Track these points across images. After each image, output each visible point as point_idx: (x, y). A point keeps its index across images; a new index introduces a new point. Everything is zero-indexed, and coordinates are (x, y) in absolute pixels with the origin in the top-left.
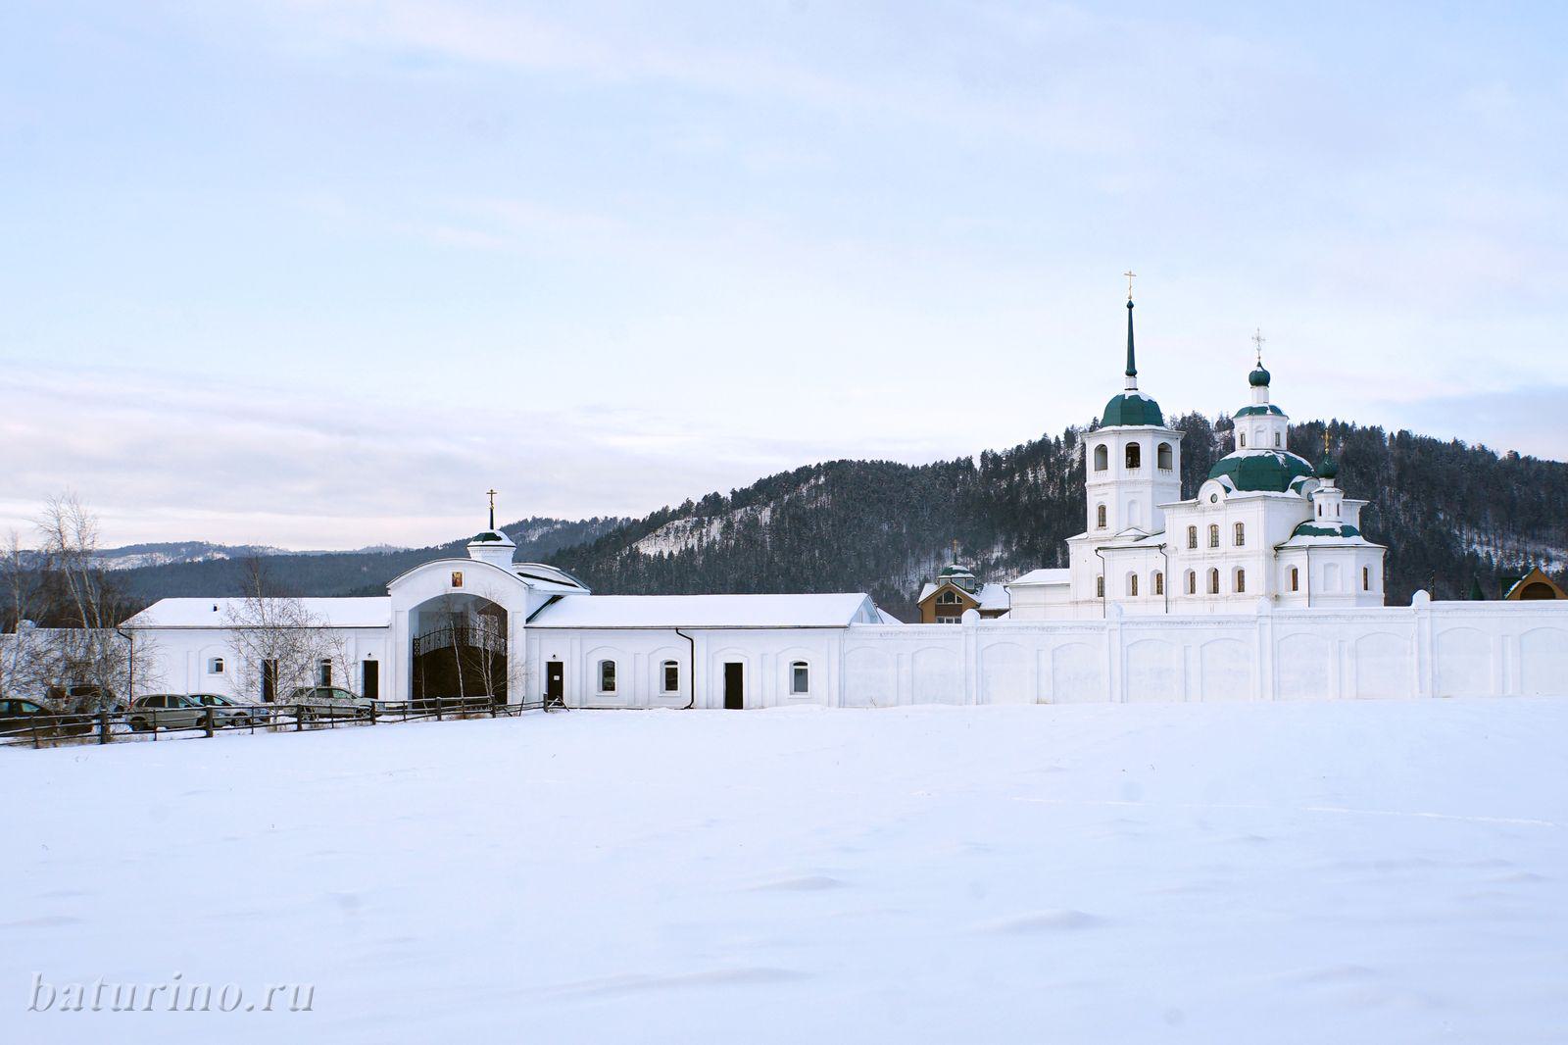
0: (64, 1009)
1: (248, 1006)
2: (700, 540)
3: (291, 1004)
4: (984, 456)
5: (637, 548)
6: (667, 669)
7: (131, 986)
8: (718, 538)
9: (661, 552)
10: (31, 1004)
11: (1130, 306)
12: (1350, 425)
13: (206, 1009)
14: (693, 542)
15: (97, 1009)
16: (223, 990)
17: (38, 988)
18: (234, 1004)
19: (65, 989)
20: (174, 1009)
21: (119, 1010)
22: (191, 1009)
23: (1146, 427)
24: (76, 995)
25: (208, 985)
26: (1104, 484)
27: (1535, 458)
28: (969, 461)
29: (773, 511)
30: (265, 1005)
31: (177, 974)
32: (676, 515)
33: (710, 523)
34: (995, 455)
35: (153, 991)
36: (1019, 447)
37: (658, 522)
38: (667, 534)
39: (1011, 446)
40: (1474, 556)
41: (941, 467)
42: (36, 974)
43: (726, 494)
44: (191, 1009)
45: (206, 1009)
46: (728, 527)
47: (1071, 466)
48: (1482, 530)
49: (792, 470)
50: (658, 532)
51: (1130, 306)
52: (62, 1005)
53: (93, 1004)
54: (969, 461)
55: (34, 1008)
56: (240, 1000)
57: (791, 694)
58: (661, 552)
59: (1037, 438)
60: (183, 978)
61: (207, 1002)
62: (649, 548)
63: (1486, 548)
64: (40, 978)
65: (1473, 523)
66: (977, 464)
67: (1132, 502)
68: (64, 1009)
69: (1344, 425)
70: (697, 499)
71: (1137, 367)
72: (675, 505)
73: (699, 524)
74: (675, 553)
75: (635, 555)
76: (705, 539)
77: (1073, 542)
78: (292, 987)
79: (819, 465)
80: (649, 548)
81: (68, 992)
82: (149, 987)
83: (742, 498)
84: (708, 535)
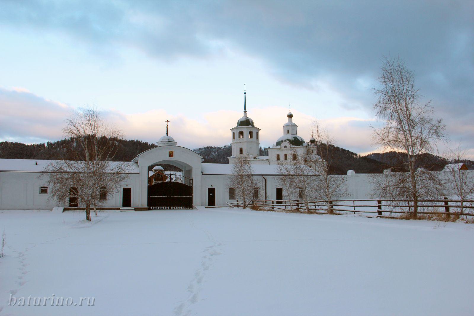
3: (88, 304)
4: (48, 143)
6: (42, 189)
7: (39, 298)
11: (245, 93)
12: (141, 141)
13: (62, 305)
15: (29, 305)
16: (68, 299)
18: (70, 304)
19: (20, 299)
22: (58, 305)
23: (246, 126)
25: (63, 298)
26: (242, 142)
27: (137, 140)
28: (44, 144)
30: (80, 304)
31: (53, 294)
34: (51, 143)
35: (82, 300)
36: (58, 142)
39: (56, 141)
44: (58, 305)
45: (62, 305)
51: (245, 93)
52: (19, 304)
53: (28, 304)
54: (44, 144)
56: (72, 302)
57: (40, 193)
59: (63, 139)
60: (55, 296)
66: (46, 145)
67: (250, 148)
68: (19, 305)
69: (139, 141)
71: (247, 110)
77: (229, 158)
81: (20, 300)
82: (45, 298)
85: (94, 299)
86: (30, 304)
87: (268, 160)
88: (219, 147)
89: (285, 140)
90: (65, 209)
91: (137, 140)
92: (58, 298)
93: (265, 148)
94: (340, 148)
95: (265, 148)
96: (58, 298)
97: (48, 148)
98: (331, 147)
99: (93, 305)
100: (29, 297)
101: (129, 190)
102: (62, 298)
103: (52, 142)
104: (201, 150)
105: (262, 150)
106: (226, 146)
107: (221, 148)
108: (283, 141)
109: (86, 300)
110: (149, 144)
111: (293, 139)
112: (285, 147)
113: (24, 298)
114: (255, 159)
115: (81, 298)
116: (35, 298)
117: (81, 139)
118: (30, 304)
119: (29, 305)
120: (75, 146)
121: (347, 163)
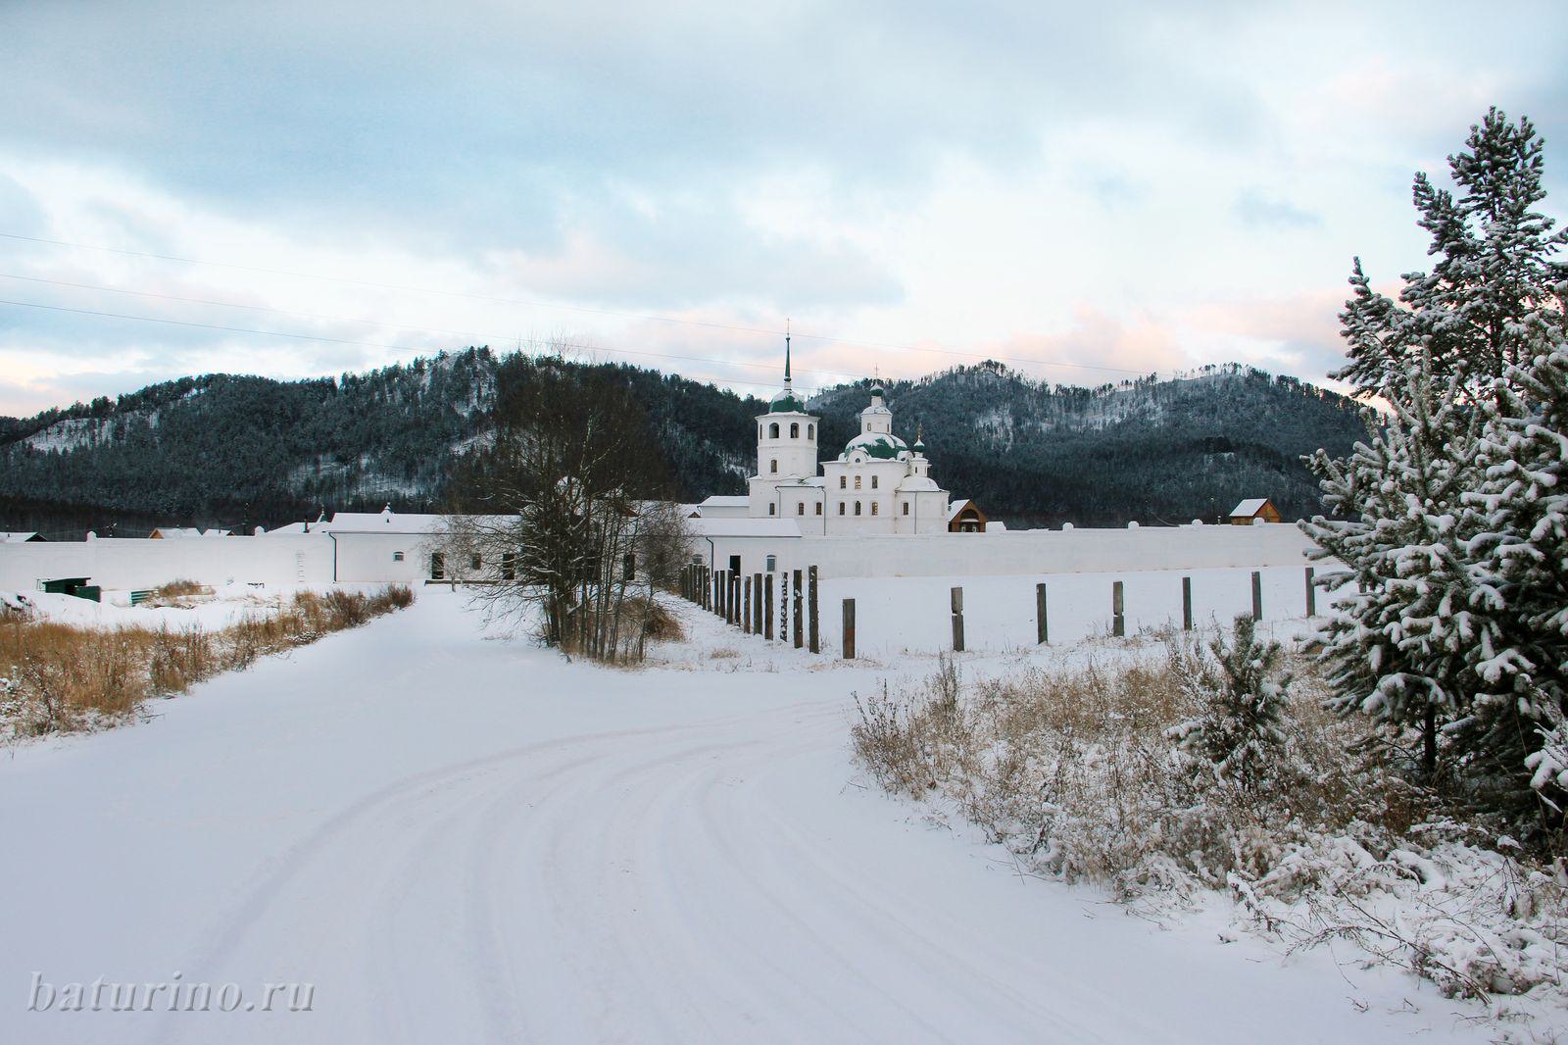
0: (64, 1009)
1: (249, 1005)
2: (93, 439)
3: (291, 1005)
4: (345, 378)
5: (31, 446)
7: (130, 986)
8: (110, 439)
9: (55, 449)
10: (31, 1004)
11: (788, 339)
12: (637, 367)
14: (86, 441)
15: (96, 1009)
16: (224, 987)
17: (38, 988)
18: (234, 1004)
19: (65, 989)
20: (174, 1009)
21: (119, 1010)
22: (191, 1009)
24: (76, 995)
25: (208, 985)
27: (625, 365)
29: (161, 417)
30: (265, 1005)
31: (177, 974)
32: (64, 415)
33: (101, 425)
34: (354, 377)
37: (48, 421)
38: (60, 432)
40: (732, 472)
41: (308, 384)
42: (36, 974)
43: (114, 399)
45: (206, 1009)
46: (118, 433)
47: (424, 391)
48: (735, 455)
49: (175, 380)
50: (49, 430)
51: (788, 339)
52: (62, 1005)
53: (93, 1004)
55: (34, 1008)
58: (55, 449)
60: (182, 978)
61: (207, 1002)
62: (43, 444)
63: (739, 468)
64: (40, 978)
65: (729, 450)
68: (64, 1009)
69: (632, 367)
70: (87, 401)
72: (65, 406)
73: (91, 426)
74: (70, 450)
75: (30, 452)
76: (97, 438)
78: (293, 987)
79: (200, 377)
80: (43, 444)
81: (68, 992)
82: (149, 987)
83: (128, 403)
84: (100, 435)
85: (312, 990)
86: (100, 1005)
87: (822, 487)
88: (904, 379)
89: (859, 446)
90: (427, 582)
91: (625, 365)
92: (191, 987)
93: (1059, 387)
94: (1317, 388)
95: (1059, 387)
96: (194, 986)
97: (346, 392)
98: (1285, 384)
99: (309, 1009)
100: (97, 983)
101: (845, 477)
102: (205, 986)
103: (359, 374)
104: (841, 393)
105: (1049, 391)
106: (926, 379)
107: (912, 383)
108: (856, 447)
109: (284, 991)
110: (663, 375)
111: (876, 444)
112: (858, 460)
113: (78, 986)
114: (800, 485)
115: (268, 987)
116: (115, 986)
117: (448, 366)
118: (100, 1005)
119: (96, 1009)
120: (428, 384)
121: (1337, 441)
